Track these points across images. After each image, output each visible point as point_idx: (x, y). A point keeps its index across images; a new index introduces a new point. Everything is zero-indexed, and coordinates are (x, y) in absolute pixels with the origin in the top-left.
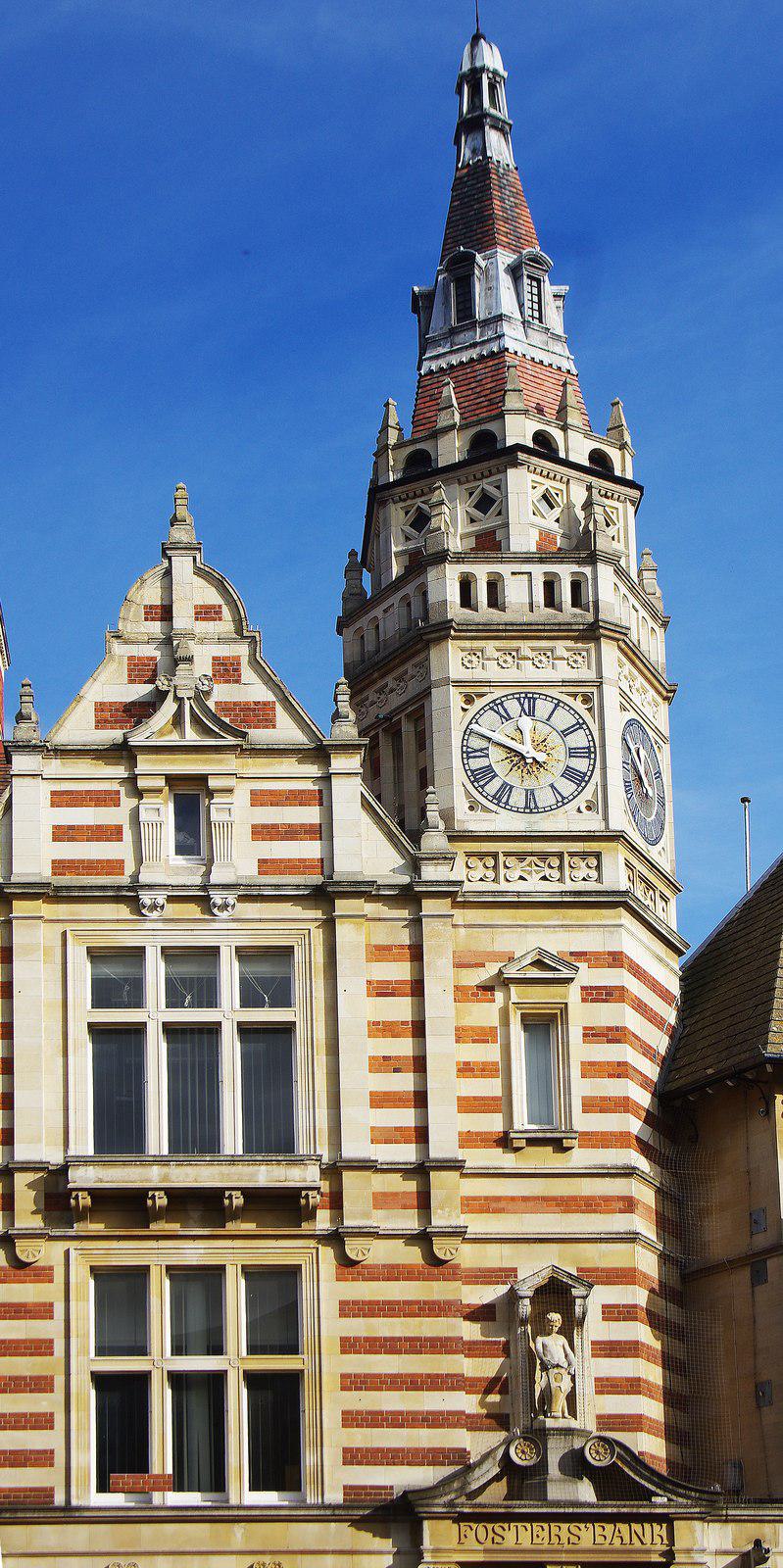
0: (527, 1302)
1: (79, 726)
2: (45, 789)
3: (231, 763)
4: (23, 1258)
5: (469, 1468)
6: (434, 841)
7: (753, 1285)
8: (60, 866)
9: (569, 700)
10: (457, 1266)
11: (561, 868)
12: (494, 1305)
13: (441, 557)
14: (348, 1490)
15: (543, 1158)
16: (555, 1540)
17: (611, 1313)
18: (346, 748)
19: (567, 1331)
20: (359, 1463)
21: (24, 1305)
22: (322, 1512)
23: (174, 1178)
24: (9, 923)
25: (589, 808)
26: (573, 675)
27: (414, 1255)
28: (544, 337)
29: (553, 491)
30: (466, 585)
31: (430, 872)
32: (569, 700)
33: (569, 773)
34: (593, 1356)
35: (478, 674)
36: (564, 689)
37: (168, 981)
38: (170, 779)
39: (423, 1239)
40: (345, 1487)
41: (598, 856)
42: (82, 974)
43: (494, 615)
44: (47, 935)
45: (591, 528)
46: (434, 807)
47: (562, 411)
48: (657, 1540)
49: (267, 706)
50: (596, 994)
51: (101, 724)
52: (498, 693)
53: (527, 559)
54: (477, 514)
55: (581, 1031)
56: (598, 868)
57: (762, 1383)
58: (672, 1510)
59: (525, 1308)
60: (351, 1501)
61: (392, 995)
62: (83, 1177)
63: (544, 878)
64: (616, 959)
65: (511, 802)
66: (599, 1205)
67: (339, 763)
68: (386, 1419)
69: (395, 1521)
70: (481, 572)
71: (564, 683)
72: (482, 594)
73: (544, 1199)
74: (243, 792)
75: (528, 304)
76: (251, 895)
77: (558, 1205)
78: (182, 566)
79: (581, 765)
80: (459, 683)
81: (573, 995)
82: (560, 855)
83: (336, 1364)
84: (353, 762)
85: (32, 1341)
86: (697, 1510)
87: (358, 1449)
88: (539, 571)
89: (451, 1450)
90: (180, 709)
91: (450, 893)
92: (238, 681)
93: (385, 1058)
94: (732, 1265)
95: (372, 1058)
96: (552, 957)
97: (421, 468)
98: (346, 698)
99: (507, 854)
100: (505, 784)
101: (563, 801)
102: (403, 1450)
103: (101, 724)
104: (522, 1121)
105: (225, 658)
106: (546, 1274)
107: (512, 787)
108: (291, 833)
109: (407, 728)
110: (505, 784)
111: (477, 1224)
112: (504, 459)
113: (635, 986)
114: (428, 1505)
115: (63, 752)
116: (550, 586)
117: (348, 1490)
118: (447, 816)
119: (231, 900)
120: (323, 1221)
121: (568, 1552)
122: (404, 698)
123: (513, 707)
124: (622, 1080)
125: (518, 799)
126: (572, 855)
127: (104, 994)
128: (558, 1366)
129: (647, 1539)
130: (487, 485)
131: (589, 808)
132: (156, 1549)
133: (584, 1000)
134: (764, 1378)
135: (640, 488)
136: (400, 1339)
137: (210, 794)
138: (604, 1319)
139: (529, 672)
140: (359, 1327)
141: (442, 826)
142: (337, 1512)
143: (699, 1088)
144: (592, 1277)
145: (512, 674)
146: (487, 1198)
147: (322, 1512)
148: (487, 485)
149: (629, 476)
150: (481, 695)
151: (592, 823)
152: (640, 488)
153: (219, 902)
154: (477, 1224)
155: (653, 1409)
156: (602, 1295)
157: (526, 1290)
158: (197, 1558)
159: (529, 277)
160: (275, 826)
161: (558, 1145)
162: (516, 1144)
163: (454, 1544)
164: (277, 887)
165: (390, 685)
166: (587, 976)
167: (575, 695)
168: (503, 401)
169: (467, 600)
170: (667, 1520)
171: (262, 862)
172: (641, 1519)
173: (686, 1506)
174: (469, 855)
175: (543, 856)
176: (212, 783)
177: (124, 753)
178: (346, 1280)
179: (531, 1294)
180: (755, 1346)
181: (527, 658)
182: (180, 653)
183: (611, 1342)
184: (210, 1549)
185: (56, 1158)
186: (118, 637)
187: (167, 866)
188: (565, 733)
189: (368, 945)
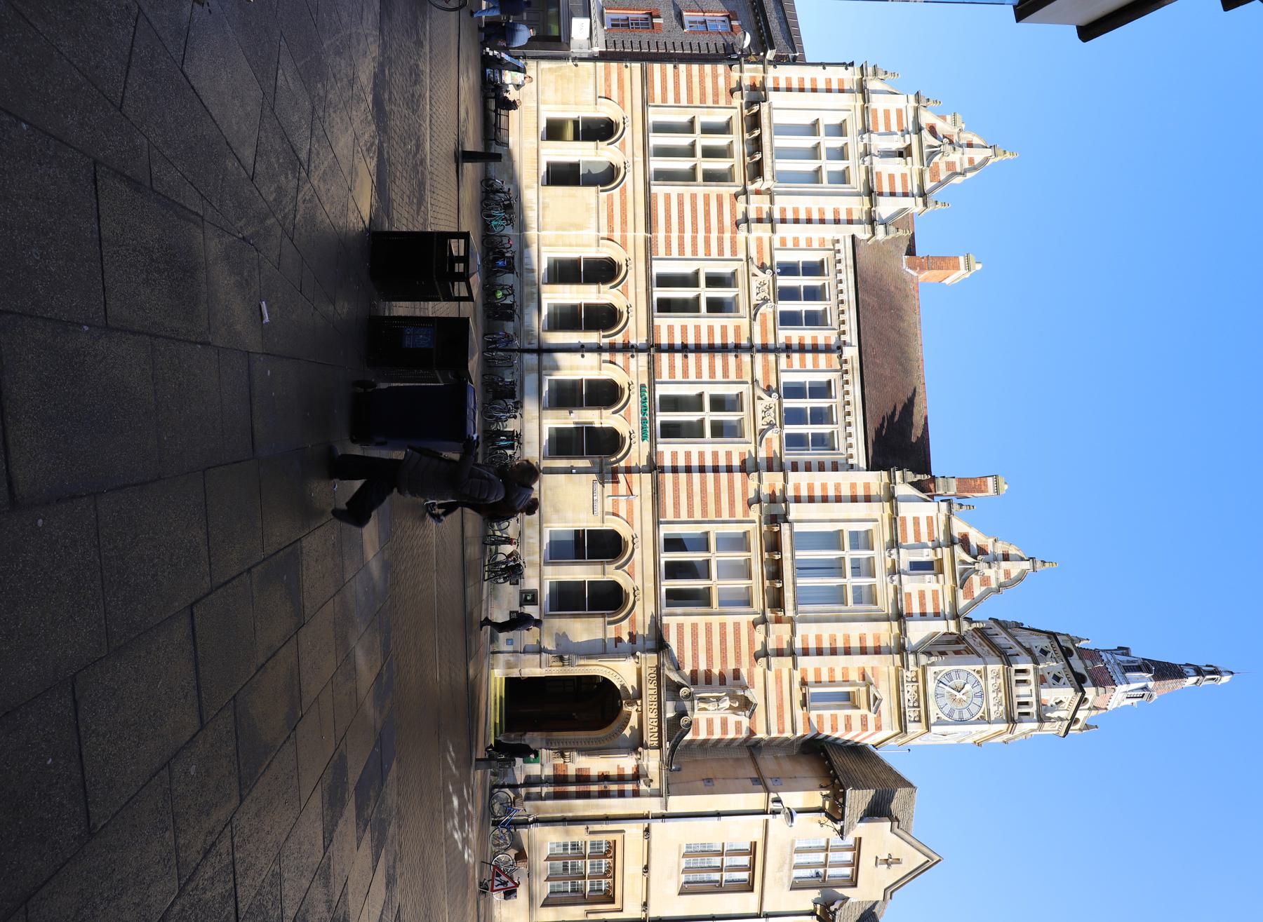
0: (743, 693)
1: (959, 528)
2: (933, 514)
3: (949, 583)
4: (752, 506)
6: (924, 659)
7: (751, 778)
8: (904, 519)
9: (982, 711)
10: (755, 666)
11: (914, 707)
12: (739, 679)
13: (1036, 662)
15: (798, 697)
16: (651, 703)
18: (959, 626)
19: (731, 708)
21: (734, 507)
24: (880, 501)
25: (938, 718)
26: (992, 713)
27: (758, 647)
28: (1120, 699)
29: (1063, 705)
30: (1024, 671)
31: (911, 658)
32: (982, 711)
33: (952, 711)
35: (990, 676)
36: (986, 710)
37: (859, 559)
38: (942, 559)
39: (765, 653)
41: (920, 721)
42: (861, 527)
43: (1014, 683)
44: (877, 515)
45: (1052, 720)
46: (936, 660)
47: (1096, 708)
48: (652, 743)
52: (982, 683)
53: (1038, 695)
54: (1052, 675)
55: (849, 714)
56: (915, 721)
59: (740, 693)
62: (785, 528)
63: (909, 700)
67: (952, 623)
70: (1030, 677)
72: (1021, 677)
73: (782, 699)
74: (938, 587)
75: (1133, 693)
78: (1026, 565)
80: (985, 669)
81: (864, 711)
82: (919, 707)
83: (715, 621)
84: (953, 629)
87: (683, 629)
88: (1033, 699)
90: (970, 564)
91: (905, 665)
93: (835, 640)
94: (758, 769)
95: (835, 635)
96: (879, 704)
97: (1067, 653)
98: (978, 626)
99: (918, 686)
101: (941, 709)
102: (683, 645)
104: (812, 690)
105: (990, 581)
106: (754, 702)
108: (922, 604)
109: (961, 647)
111: (771, 675)
112: (1078, 687)
115: (949, 519)
118: (933, 664)
119: (895, 583)
120: (769, 614)
121: (647, 708)
122: (973, 645)
124: (830, 730)
126: (919, 711)
127: (854, 534)
128: (718, 706)
129: (652, 739)
130: (1064, 679)
131: (938, 718)
133: (862, 716)
134: (715, 782)
135: (1064, 736)
137: (936, 575)
138: (736, 722)
139: (992, 695)
140: (730, 630)
141: (929, 662)
143: (828, 758)
145: (991, 689)
146: (781, 677)
148: (1064, 679)
149: (1070, 732)
150: (981, 677)
151: (933, 719)
152: (1064, 736)
153: (894, 578)
154: (771, 675)
155: (703, 736)
157: (747, 694)
159: (1144, 694)
160: (924, 598)
161: (804, 704)
162: (804, 689)
163: (648, 665)
164: (901, 600)
165: (977, 640)
167: (983, 713)
168: (1101, 686)
169: (1018, 671)
170: (660, 747)
171: (910, 594)
172: (660, 736)
174: (917, 672)
175: (918, 700)
176: (941, 576)
177: (951, 542)
179: (746, 695)
181: (997, 694)
182: (992, 564)
183: (727, 724)
185: (790, 518)
186: (995, 540)
187: (906, 558)
188: (969, 710)
189: (880, 634)
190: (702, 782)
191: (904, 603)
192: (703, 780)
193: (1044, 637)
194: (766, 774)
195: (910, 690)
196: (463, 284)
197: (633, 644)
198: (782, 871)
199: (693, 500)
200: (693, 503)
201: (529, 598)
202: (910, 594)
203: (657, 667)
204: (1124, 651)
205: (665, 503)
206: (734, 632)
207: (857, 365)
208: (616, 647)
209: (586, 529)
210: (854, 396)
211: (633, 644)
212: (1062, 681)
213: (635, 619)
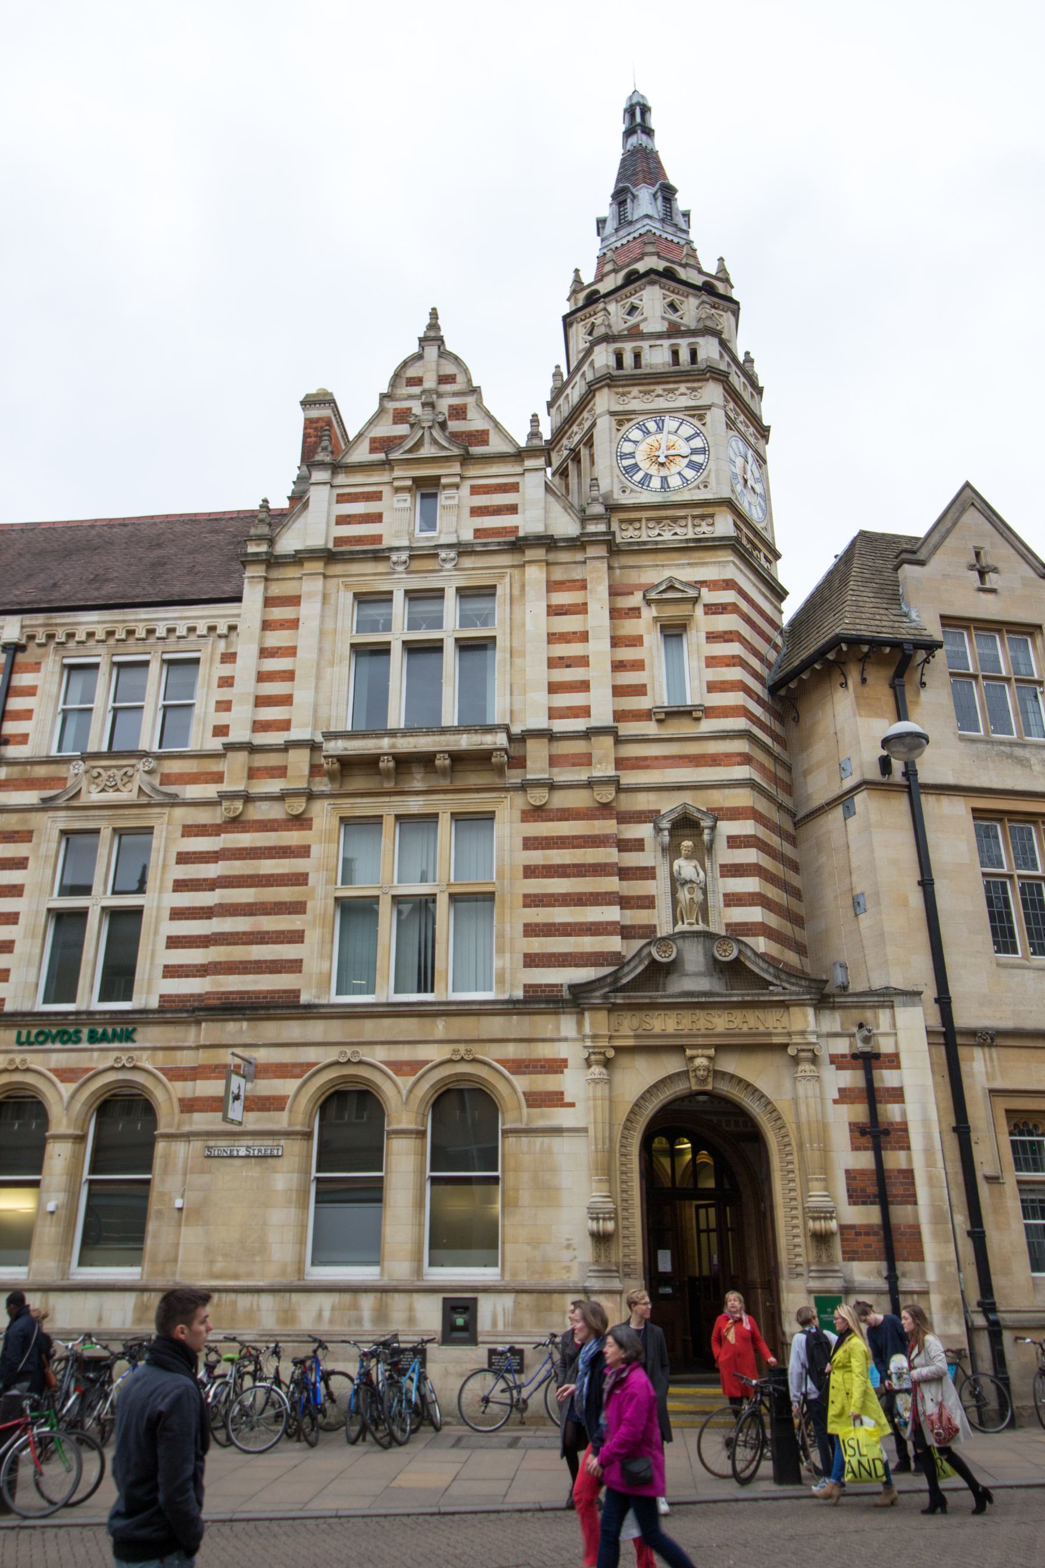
0: (666, 833)
5: (622, 966)
7: (845, 819)
14: (527, 987)
17: (735, 842)
20: (537, 966)
21: (289, 847)
22: (505, 1007)
23: (399, 746)
28: (674, 229)
34: (722, 876)
40: (525, 986)
49: (485, 433)
50: (712, 609)
51: (372, 450)
52: (641, 418)
53: (659, 336)
57: (857, 896)
58: (787, 998)
60: (530, 997)
61: (565, 614)
64: (729, 584)
65: (651, 485)
66: (721, 760)
68: (559, 930)
69: (564, 1013)
71: (688, 408)
76: (463, 550)
77: (691, 762)
79: (699, 458)
81: (699, 610)
85: (294, 874)
86: (808, 997)
89: (608, 953)
92: (465, 419)
96: (681, 582)
100: (647, 474)
103: (372, 450)
107: (651, 476)
110: (647, 474)
113: (744, 606)
114: (587, 998)
116: (675, 353)
117: (527, 987)
123: (651, 426)
125: (656, 483)
130: (634, 300)
132: (375, 1039)
133: (706, 613)
134: (858, 891)
136: (569, 866)
140: (538, 857)
142: (517, 1006)
144: (719, 814)
147: (505, 1007)
156: (728, 828)
158: (407, 1046)
164: (485, 544)
166: (709, 596)
167: (693, 416)
171: (476, 531)
173: (798, 994)
178: (529, 821)
180: (850, 866)
184: (417, 1039)
188: (688, 439)
190: (861, 917)
191: (490, 540)
192: (856, 915)
193: (572, 331)
194: (835, 791)
195: (657, 532)
196: (95, 1454)
197: (566, 1067)
198: (1028, 760)
199: (268, 932)
200: (273, 932)
201: (460, 1321)
202: (477, 531)
203: (610, 1011)
204: (601, 223)
205: (269, 992)
206: (543, 849)
207: (40, 618)
208: (572, 1105)
209: (314, 1174)
210: (99, 622)
211: (566, 1067)
212: (637, 302)
213: (514, 1061)
